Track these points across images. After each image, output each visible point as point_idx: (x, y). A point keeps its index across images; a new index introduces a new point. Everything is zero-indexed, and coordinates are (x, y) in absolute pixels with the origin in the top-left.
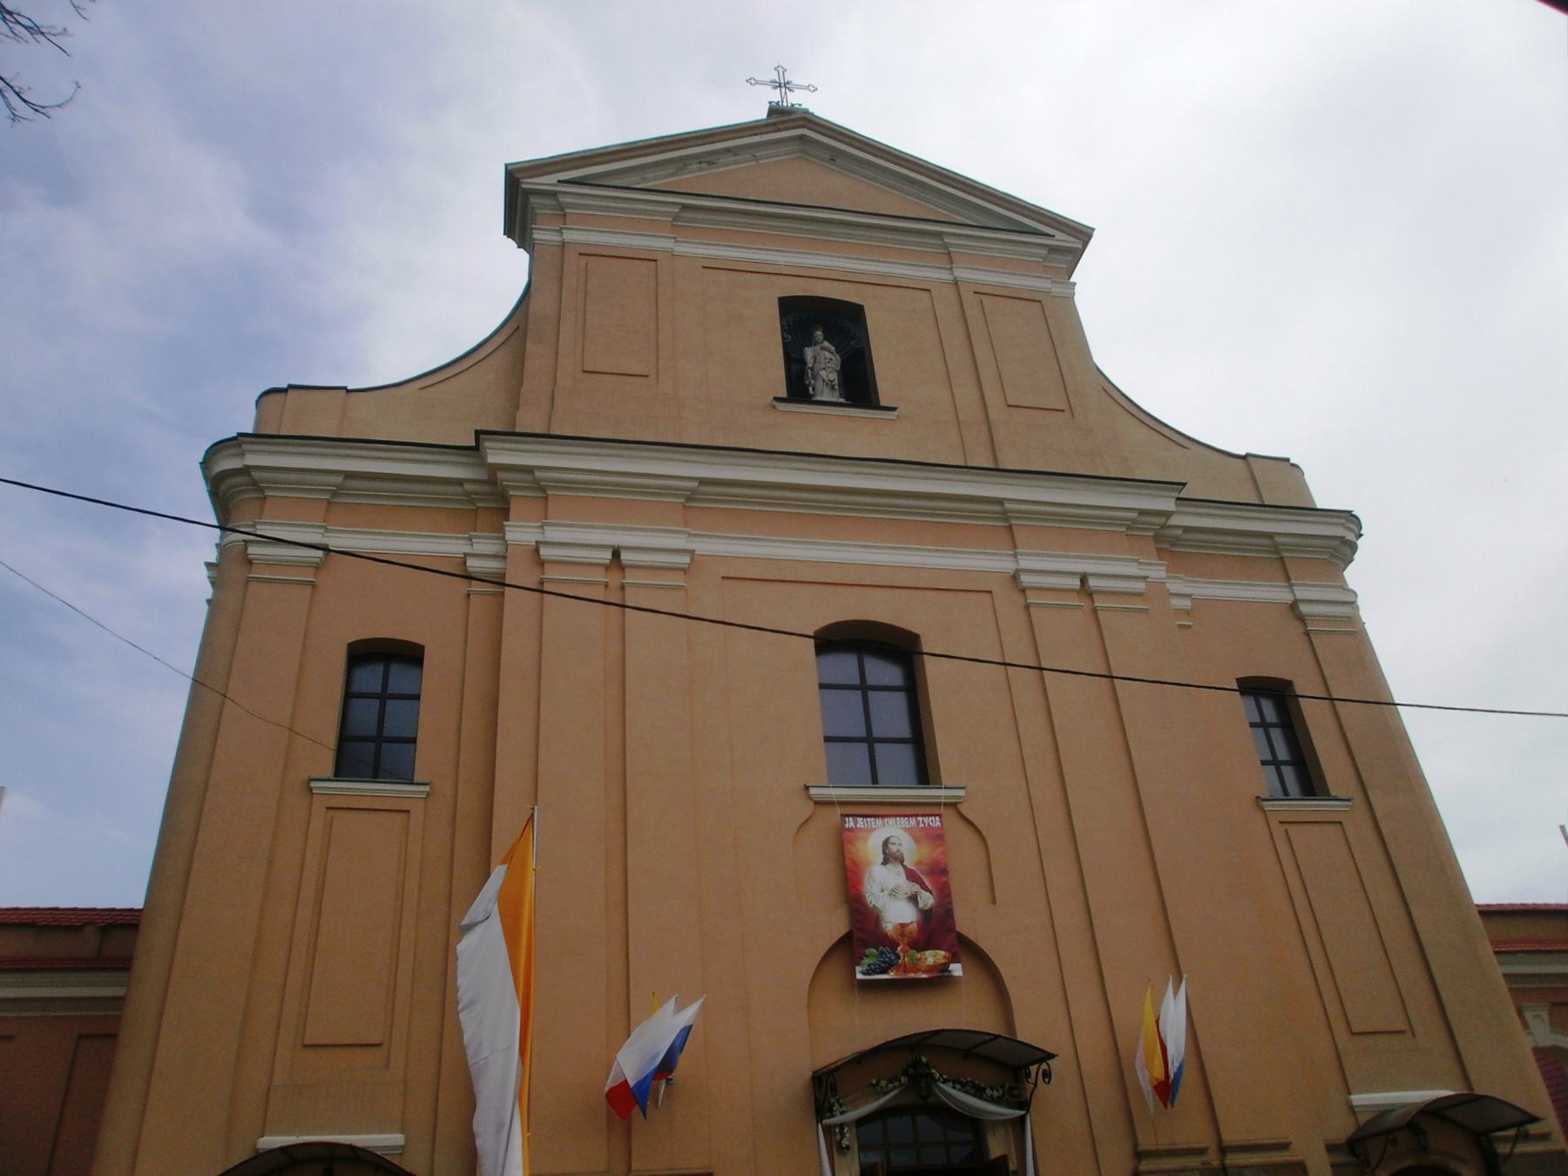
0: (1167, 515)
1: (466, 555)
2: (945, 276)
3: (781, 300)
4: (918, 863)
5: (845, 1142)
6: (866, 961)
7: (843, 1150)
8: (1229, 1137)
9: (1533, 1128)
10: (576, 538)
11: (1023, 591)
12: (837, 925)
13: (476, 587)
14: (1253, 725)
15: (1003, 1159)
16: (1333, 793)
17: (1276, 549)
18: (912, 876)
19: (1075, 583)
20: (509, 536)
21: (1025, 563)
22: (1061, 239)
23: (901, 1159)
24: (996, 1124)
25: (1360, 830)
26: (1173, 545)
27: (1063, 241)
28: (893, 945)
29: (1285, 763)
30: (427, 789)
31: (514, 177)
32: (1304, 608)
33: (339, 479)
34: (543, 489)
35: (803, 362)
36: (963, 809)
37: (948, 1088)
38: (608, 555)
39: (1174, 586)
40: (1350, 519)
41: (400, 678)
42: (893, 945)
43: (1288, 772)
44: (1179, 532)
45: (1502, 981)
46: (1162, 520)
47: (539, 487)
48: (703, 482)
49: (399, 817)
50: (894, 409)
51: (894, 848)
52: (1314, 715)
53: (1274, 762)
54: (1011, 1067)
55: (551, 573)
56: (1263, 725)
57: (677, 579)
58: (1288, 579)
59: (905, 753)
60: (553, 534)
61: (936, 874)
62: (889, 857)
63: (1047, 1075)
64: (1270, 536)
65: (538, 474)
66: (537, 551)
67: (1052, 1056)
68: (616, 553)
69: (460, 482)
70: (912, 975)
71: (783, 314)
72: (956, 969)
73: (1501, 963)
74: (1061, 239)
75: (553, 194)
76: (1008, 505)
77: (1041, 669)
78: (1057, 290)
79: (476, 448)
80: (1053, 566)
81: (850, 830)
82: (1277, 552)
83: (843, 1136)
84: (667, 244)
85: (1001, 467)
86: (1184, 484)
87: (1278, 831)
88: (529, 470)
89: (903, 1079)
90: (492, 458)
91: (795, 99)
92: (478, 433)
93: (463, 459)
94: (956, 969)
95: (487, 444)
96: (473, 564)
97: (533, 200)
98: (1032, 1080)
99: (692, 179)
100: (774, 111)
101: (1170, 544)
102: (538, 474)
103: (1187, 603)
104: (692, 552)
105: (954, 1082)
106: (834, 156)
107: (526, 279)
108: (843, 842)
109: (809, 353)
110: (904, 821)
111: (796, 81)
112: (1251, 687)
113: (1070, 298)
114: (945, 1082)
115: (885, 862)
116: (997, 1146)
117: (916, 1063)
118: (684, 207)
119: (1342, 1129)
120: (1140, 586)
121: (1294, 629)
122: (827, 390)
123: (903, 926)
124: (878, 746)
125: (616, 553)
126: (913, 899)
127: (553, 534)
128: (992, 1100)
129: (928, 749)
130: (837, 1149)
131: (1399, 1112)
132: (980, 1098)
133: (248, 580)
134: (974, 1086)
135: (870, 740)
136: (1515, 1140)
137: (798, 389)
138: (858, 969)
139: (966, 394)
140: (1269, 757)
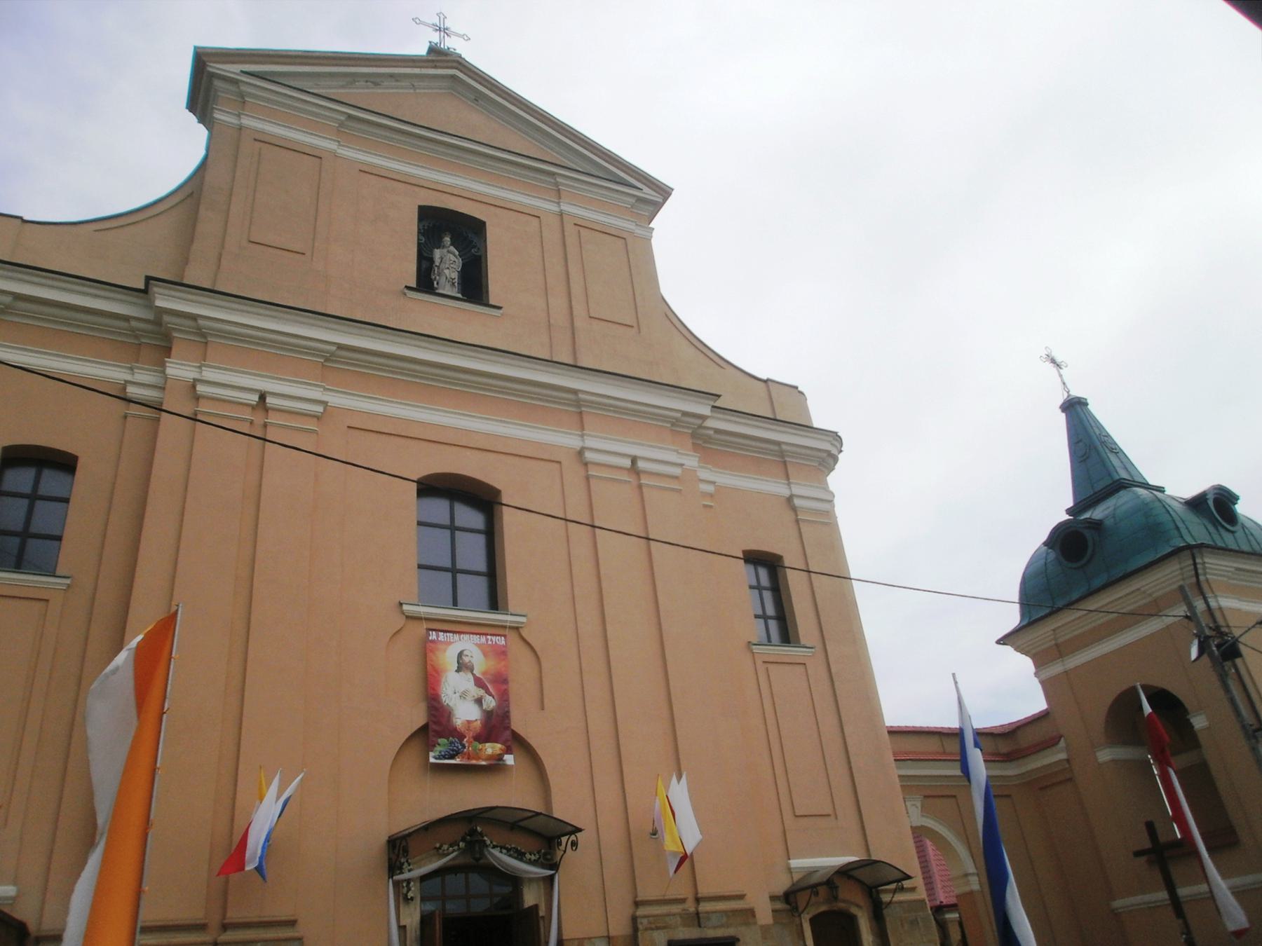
0: (704, 418)
1: (126, 382)
2: (554, 208)
3: (420, 207)
4: (484, 673)
5: (410, 895)
6: (438, 748)
7: (408, 900)
8: (703, 891)
9: (906, 884)
10: (230, 381)
11: (586, 464)
12: (418, 717)
13: (134, 410)
14: (751, 587)
15: (536, 907)
16: (803, 642)
17: (782, 454)
18: (479, 683)
19: (627, 463)
20: (169, 371)
21: (590, 443)
22: (647, 193)
23: (453, 908)
24: (531, 880)
25: (817, 669)
26: (705, 442)
27: (648, 195)
28: (461, 736)
29: (771, 618)
30: (68, 581)
31: (203, 62)
32: (797, 502)
33: (679, 415)
34: (204, 335)
35: (431, 260)
36: (524, 633)
37: (496, 852)
38: (256, 398)
39: (704, 474)
40: (835, 438)
41: (51, 482)
43: (773, 625)
44: (711, 432)
45: (897, 780)
46: (699, 422)
47: (201, 333)
48: (341, 347)
49: (42, 604)
50: (499, 308)
51: (466, 659)
52: (795, 582)
53: (764, 617)
54: (547, 838)
55: (204, 407)
56: (758, 587)
57: (311, 425)
58: (788, 478)
59: (481, 584)
60: (209, 374)
61: (498, 683)
62: (462, 666)
63: (575, 844)
65: (201, 322)
66: (194, 387)
67: (580, 830)
68: (263, 397)
69: (126, 318)
70: (474, 762)
71: (420, 219)
72: (509, 759)
73: (898, 768)
74: (647, 193)
76: (581, 396)
77: (594, 526)
78: (639, 231)
79: (145, 291)
80: (610, 447)
81: (433, 641)
82: (783, 457)
83: (409, 890)
84: (332, 146)
85: (579, 364)
86: (719, 396)
87: (761, 668)
88: (194, 317)
89: (462, 844)
90: (159, 303)
91: (451, 44)
92: (148, 279)
93: (134, 300)
94: (509, 759)
95: (156, 289)
96: (132, 391)
97: (217, 83)
98: (563, 847)
99: (357, 94)
100: (433, 50)
101: (702, 440)
102: (201, 322)
103: (710, 489)
104: (325, 403)
105: (501, 848)
106: (478, 97)
107: (200, 153)
108: (426, 651)
109: (437, 253)
110: (476, 638)
111: (453, 29)
112: (754, 558)
113: (648, 240)
114: (494, 847)
115: (458, 671)
116: (530, 897)
117: (473, 832)
118: (350, 117)
119: (782, 884)
120: (677, 471)
121: (788, 516)
122: (448, 286)
123: (469, 722)
124: (459, 576)
125: (263, 397)
126: (479, 701)
127: (209, 374)
128: (530, 862)
129: (499, 583)
130: (403, 899)
131: (821, 872)
132: (521, 860)
134: (517, 851)
135: (454, 571)
136: (894, 891)
137: (425, 283)
138: (431, 754)
139: (558, 304)
140: (760, 612)
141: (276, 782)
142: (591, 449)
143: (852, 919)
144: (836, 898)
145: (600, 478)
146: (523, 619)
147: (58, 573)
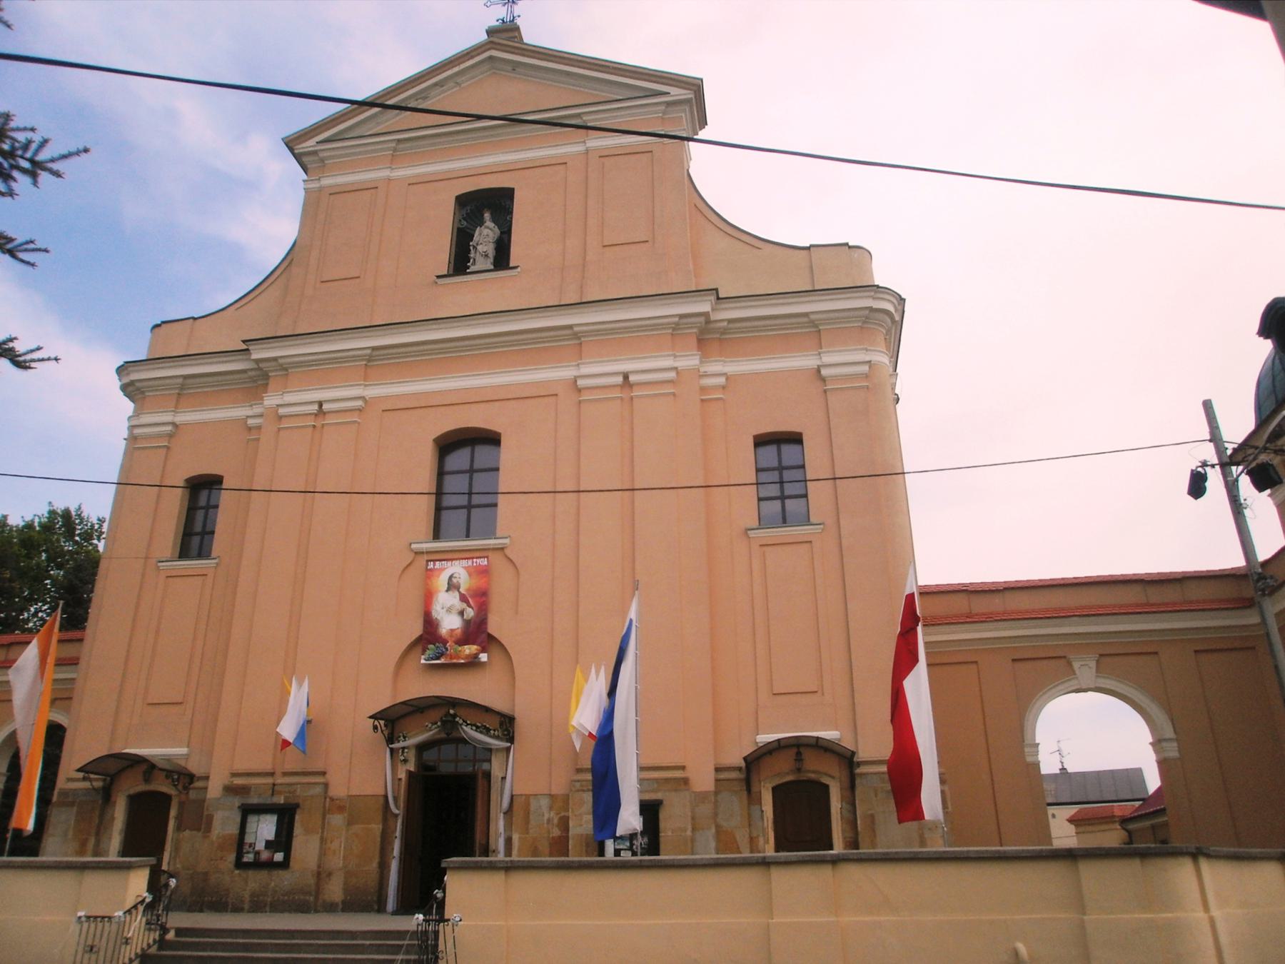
0: (706, 315)
4: (468, 590)
10: (294, 398)
12: (417, 630)
18: (463, 598)
19: (620, 379)
24: (498, 750)
26: (723, 333)
28: (445, 642)
33: (676, 319)
37: (467, 729)
41: (483, 454)
42: (445, 642)
57: (355, 417)
61: (480, 599)
62: (452, 586)
64: (806, 315)
68: (626, 376)
72: (484, 657)
74: (676, 93)
75: (315, 153)
76: (576, 329)
80: (599, 369)
88: (275, 359)
94: (484, 657)
101: (708, 336)
102: (281, 361)
104: (363, 398)
110: (464, 562)
123: (452, 630)
125: (626, 376)
126: (461, 613)
128: (497, 738)
133: (279, 429)
137: (460, 263)
141: (593, 670)
142: (632, 372)
143: (826, 788)
144: (799, 770)
145: (641, 396)
146: (506, 541)
147: (813, 520)
